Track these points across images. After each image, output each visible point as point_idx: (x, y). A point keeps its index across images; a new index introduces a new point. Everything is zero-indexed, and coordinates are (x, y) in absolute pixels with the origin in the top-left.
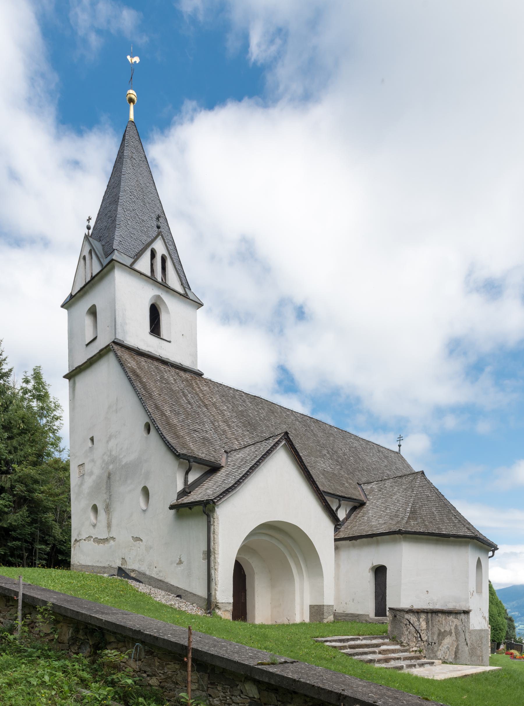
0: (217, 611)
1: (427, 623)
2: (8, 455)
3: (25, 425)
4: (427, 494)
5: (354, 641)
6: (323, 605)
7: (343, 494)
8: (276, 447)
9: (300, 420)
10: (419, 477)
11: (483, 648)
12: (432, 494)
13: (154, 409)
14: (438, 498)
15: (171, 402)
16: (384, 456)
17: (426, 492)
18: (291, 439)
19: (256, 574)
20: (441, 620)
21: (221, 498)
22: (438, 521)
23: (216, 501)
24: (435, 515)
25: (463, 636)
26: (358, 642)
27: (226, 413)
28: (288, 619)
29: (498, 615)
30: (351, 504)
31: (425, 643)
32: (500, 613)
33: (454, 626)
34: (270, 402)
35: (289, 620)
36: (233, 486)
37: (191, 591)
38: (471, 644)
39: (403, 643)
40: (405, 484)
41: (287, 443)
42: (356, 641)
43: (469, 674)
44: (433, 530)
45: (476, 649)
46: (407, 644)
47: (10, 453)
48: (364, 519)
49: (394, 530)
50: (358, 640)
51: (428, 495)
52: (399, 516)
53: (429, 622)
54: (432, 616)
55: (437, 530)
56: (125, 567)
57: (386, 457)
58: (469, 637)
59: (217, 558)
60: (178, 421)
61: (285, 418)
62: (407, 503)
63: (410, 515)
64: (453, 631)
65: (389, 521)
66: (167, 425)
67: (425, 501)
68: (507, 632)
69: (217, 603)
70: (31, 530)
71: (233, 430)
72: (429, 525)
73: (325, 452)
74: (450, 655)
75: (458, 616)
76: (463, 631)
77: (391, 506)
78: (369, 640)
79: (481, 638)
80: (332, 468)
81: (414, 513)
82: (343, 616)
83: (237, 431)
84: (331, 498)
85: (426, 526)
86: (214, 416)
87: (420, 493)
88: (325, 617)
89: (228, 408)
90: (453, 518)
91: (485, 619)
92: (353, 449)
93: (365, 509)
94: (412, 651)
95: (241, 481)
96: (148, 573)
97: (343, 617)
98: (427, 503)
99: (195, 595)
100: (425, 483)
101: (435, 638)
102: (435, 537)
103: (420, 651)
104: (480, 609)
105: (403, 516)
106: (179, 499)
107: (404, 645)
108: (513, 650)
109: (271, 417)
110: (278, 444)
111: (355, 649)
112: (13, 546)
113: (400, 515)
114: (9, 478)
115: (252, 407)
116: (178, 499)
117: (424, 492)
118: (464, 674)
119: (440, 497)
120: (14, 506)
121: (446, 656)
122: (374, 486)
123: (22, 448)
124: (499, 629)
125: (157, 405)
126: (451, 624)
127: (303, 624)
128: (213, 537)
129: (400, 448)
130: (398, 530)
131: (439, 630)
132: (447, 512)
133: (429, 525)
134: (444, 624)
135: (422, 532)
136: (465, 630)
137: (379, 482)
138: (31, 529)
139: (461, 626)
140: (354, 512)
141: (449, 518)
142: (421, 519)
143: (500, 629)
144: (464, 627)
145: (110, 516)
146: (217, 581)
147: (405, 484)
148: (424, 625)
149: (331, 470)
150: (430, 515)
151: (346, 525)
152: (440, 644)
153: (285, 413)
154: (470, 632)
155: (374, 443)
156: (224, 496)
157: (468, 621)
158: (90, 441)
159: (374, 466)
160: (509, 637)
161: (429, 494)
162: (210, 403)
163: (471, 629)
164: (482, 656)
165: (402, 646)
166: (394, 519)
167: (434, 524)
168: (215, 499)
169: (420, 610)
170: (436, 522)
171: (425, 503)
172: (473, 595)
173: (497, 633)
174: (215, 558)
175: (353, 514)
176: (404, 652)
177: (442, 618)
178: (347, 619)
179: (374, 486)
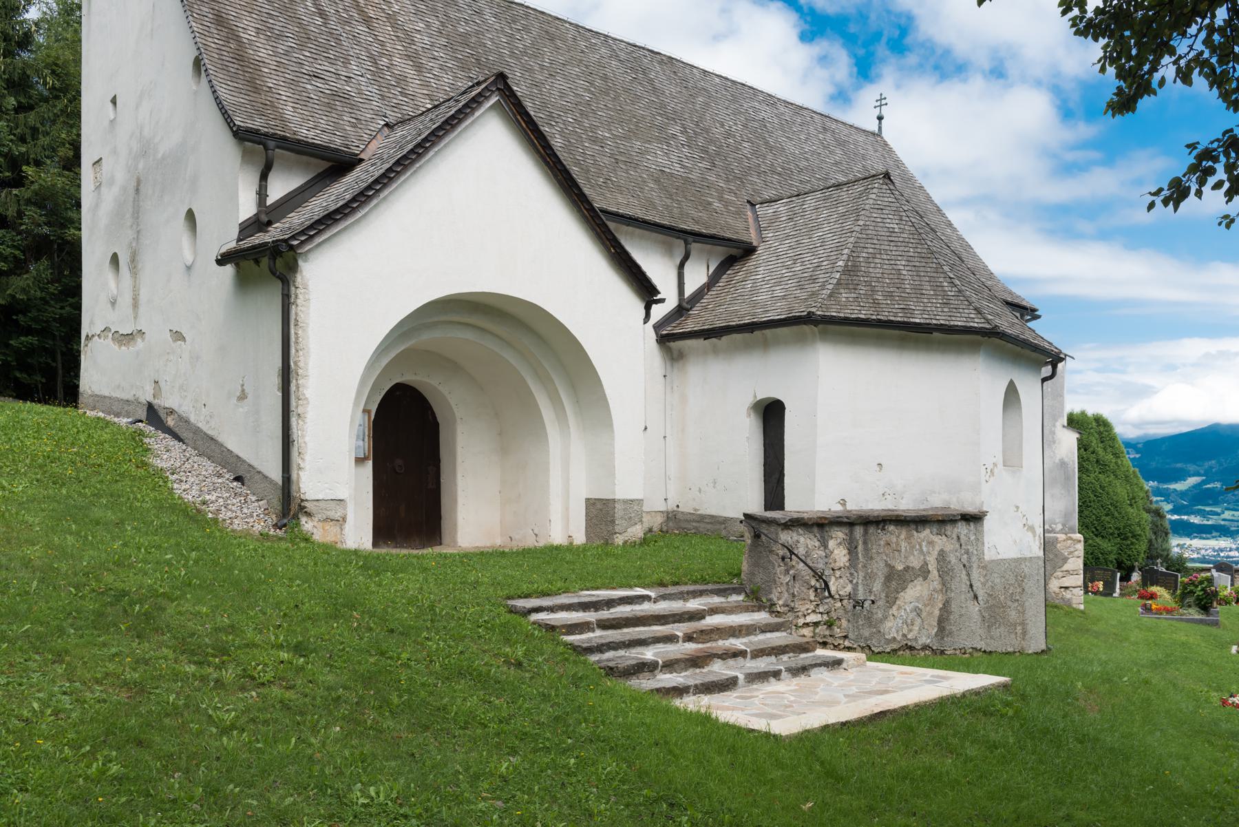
0: (303, 519)
1: (852, 551)
2: (17, 145)
3: (58, 80)
4: (892, 226)
5: (630, 603)
6: (614, 501)
7: (696, 228)
8: (473, 110)
9: (623, 56)
10: (876, 186)
11: (1027, 604)
12: (902, 227)
13: (209, 24)
14: (916, 237)
15: (267, 11)
16: (836, 140)
17: (888, 221)
18: (519, 94)
19: (458, 421)
21: (311, 237)
22: (908, 291)
23: (295, 243)
24: (902, 277)
25: (964, 577)
26: (646, 608)
27: (418, 36)
28: (536, 532)
29: (1128, 502)
30: (721, 253)
31: (845, 602)
32: (1134, 498)
33: (936, 553)
34: (550, 15)
35: (536, 535)
36: (346, 205)
37: (260, 468)
39: (775, 604)
40: (845, 204)
41: (506, 102)
42: (636, 603)
43: (896, 707)
44: (891, 314)
45: (1003, 607)
46: (786, 608)
47: (22, 139)
48: (746, 287)
49: (797, 314)
50: (644, 601)
51: (891, 230)
52: (817, 281)
53: (856, 547)
54: (866, 532)
55: (900, 315)
56: (159, 401)
57: (842, 143)
58: (982, 580)
59: (303, 386)
60: (271, 53)
61: (582, 52)
62: (841, 248)
63: (843, 277)
64: (932, 567)
65: (795, 292)
66: (234, 61)
67: (882, 243)
68: (1150, 541)
69: (302, 500)
70: (63, 311)
71: (428, 75)
72: (885, 302)
73: (675, 129)
75: (949, 528)
76: (964, 566)
77: (805, 255)
78: (680, 599)
80: (684, 167)
81: (852, 273)
82: (694, 521)
83: (437, 77)
84: (665, 237)
85: (875, 305)
86: (382, 44)
87: (874, 224)
88: (617, 531)
89: (428, 25)
90: (946, 284)
92: (756, 124)
93: (751, 263)
94: (804, 624)
95: (371, 193)
96: (193, 419)
97: (694, 524)
98: (888, 248)
99: (267, 477)
100: (890, 200)
101: (877, 586)
102: (897, 332)
103: (830, 625)
104: (1017, 507)
105: (825, 280)
106: (241, 240)
107: (779, 609)
108: (1157, 585)
109: (545, 49)
110: (480, 104)
111: (620, 628)
112: (21, 346)
113: (820, 276)
114: (16, 195)
115: (497, 26)
116: (239, 240)
117: (885, 221)
118: (877, 710)
119: (920, 234)
120: (23, 257)
121: (911, 631)
122: (781, 209)
123: (48, 130)
125: (224, 15)
126: (925, 549)
127: (570, 548)
128: (296, 334)
129: (880, 123)
130: (805, 313)
131: (887, 565)
132: (933, 270)
133: (885, 302)
134: (903, 550)
135: (863, 320)
136: (969, 562)
137: (794, 199)
138: (62, 308)
139: (958, 554)
140: (728, 270)
141: (935, 284)
142: (868, 288)
144: (965, 556)
145: (137, 282)
146: (303, 445)
147: (845, 204)
148: (840, 555)
149: (682, 170)
150: (891, 276)
151: (705, 301)
152: (891, 601)
153: (587, 40)
154: (984, 567)
155: (815, 112)
156: (320, 232)
157: (979, 540)
158: (110, 105)
159: (803, 164)
160: (1154, 553)
161: (896, 226)
162: (383, 15)
163: (987, 558)
164: (1023, 624)
165: (773, 612)
166: (806, 287)
167: (897, 298)
168: (293, 237)
169: (825, 518)
170: (903, 295)
171: (883, 247)
173: (1128, 545)
174: (298, 387)
175: (725, 274)
176: (770, 631)
178: (701, 529)
179: (781, 209)
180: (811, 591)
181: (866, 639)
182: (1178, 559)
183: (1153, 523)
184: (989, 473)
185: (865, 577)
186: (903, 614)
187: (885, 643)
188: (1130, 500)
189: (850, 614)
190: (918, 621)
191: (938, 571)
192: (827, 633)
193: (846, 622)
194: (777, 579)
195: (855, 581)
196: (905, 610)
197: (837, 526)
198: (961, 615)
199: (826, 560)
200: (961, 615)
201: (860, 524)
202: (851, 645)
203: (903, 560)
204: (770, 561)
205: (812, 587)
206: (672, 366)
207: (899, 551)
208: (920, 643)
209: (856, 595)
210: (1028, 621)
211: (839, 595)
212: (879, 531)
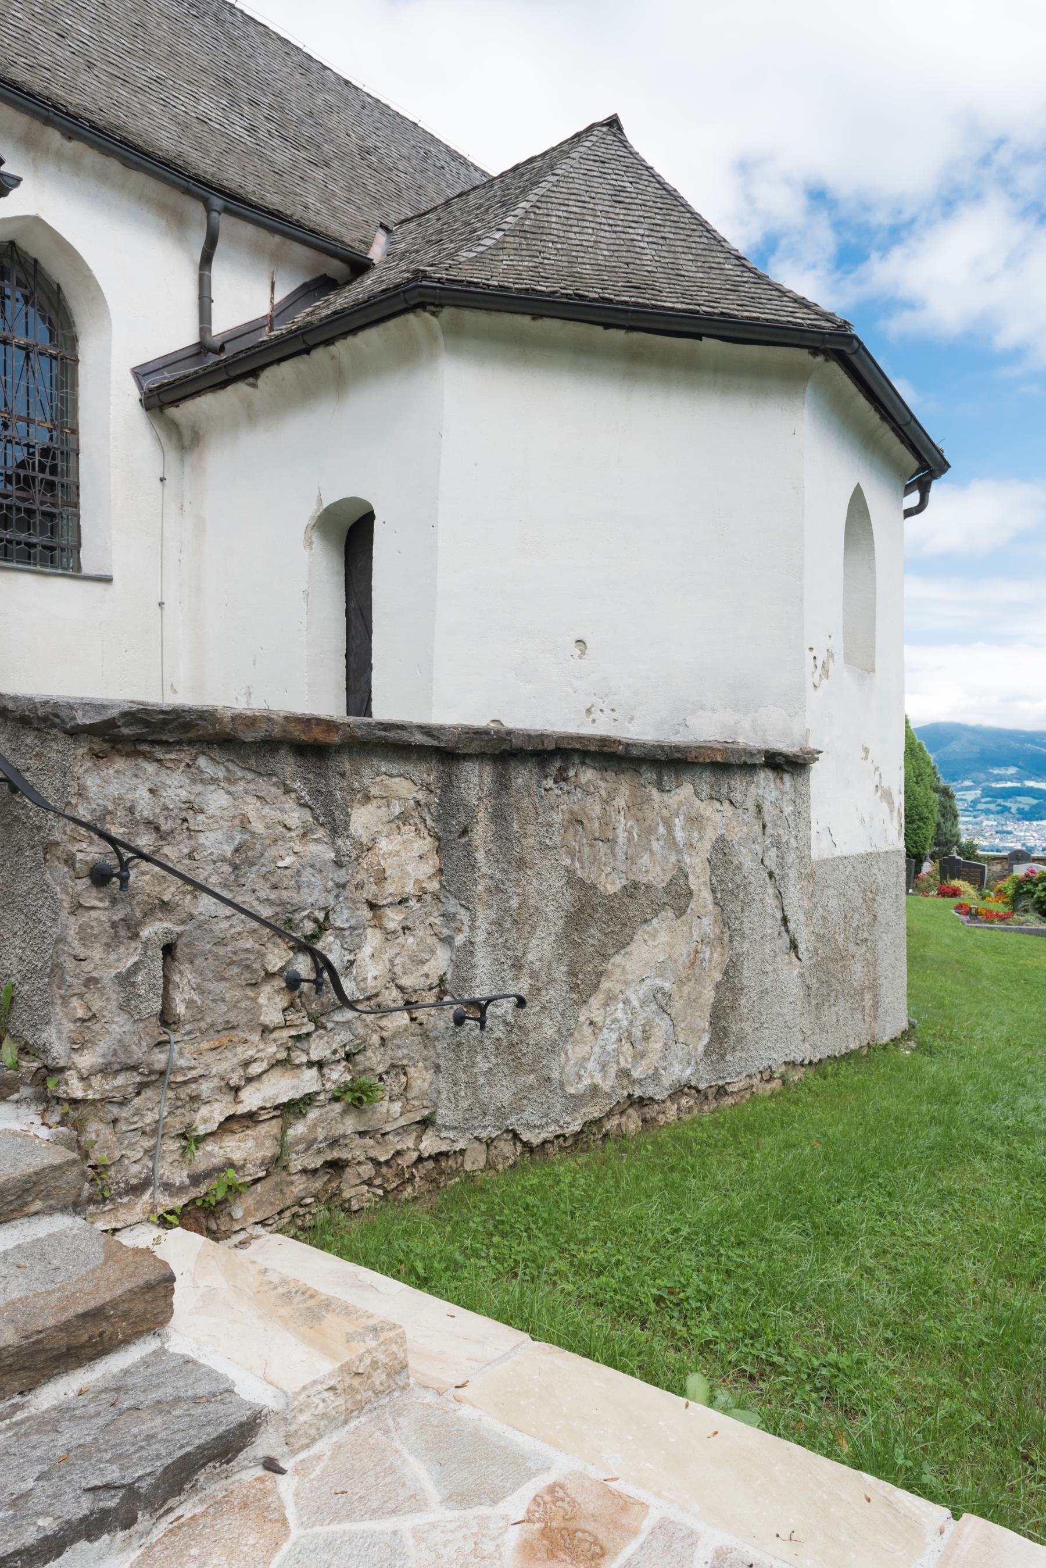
11: (880, 944)
20: (596, 810)
25: (771, 901)
32: (920, 775)
33: (708, 845)
38: (820, 937)
53: (465, 832)
54: (502, 785)
58: (806, 904)
64: (699, 882)
68: (938, 825)
74: (672, 1040)
75: (738, 782)
76: (771, 875)
79: (871, 894)
91: (891, 803)
104: (866, 750)
107: (76, 1089)
124: (917, 817)
126: (679, 835)
131: (573, 881)
136: (781, 865)
143: (921, 819)
144: (773, 852)
154: (810, 877)
157: (801, 815)
163: (815, 854)
164: (874, 987)
172: (826, 673)
177: (607, 802)
180: (267, 989)
181: (501, 1113)
182: (967, 845)
183: (941, 804)
184: (819, 670)
185: (498, 923)
186: (619, 1014)
187: (566, 1110)
188: (917, 777)
189: (440, 1046)
190: (663, 1024)
191: (713, 891)
192: (350, 1125)
193: (429, 1075)
194: (70, 964)
195: (460, 939)
196: (626, 1002)
197: (385, 758)
198: (764, 992)
199: (341, 876)
200: (764, 992)
201: (480, 756)
202: (444, 1148)
203: (623, 868)
204: (44, 888)
205: (269, 976)
206: (182, 460)
207: (611, 842)
208: (666, 1081)
209: (464, 981)
210: (882, 980)
211: (401, 989)
212: (550, 783)
